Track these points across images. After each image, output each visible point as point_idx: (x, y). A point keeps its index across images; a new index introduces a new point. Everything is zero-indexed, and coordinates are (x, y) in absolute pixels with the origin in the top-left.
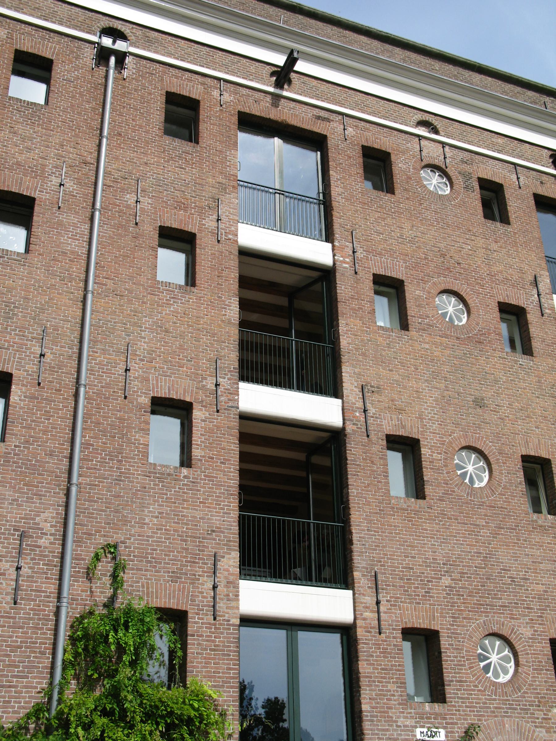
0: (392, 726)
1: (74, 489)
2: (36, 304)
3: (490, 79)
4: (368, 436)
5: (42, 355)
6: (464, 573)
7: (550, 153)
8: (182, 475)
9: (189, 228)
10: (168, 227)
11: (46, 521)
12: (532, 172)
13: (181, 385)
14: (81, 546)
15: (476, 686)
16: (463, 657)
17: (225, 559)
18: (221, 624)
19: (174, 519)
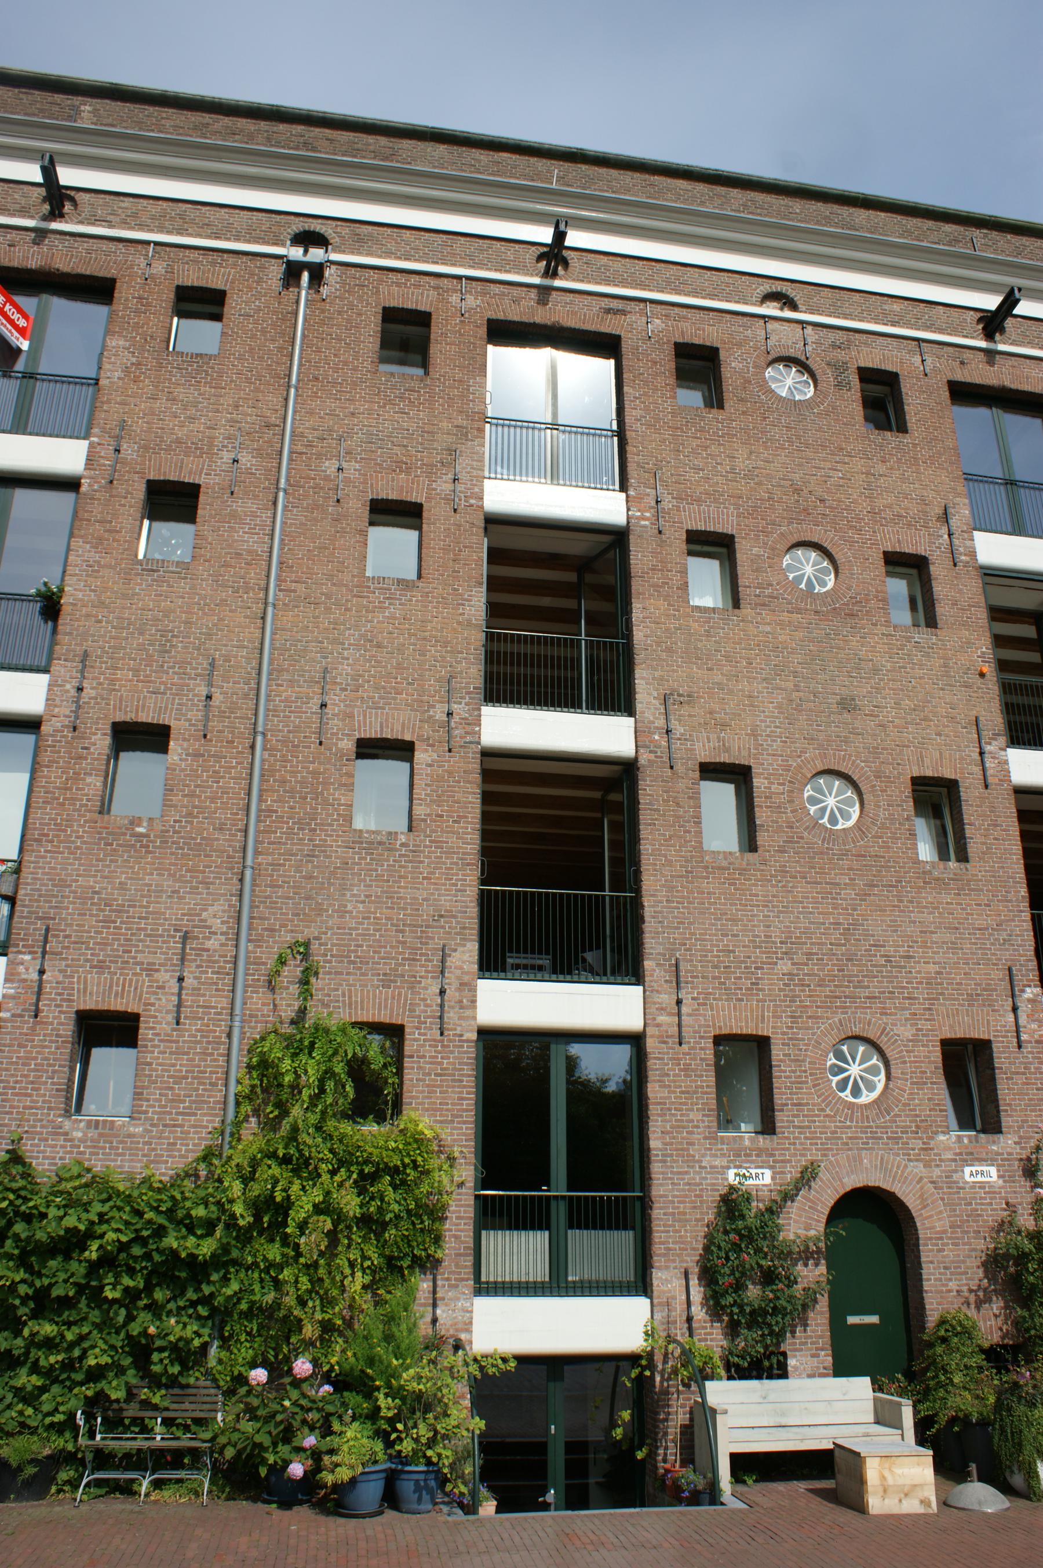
1: (248, 873)
3: (883, 214)
4: (672, 767)
5: (209, 697)
7: (979, 315)
9: (413, 497)
11: (215, 916)
12: (945, 348)
14: (261, 947)
15: (823, 1110)
18: (450, 1041)
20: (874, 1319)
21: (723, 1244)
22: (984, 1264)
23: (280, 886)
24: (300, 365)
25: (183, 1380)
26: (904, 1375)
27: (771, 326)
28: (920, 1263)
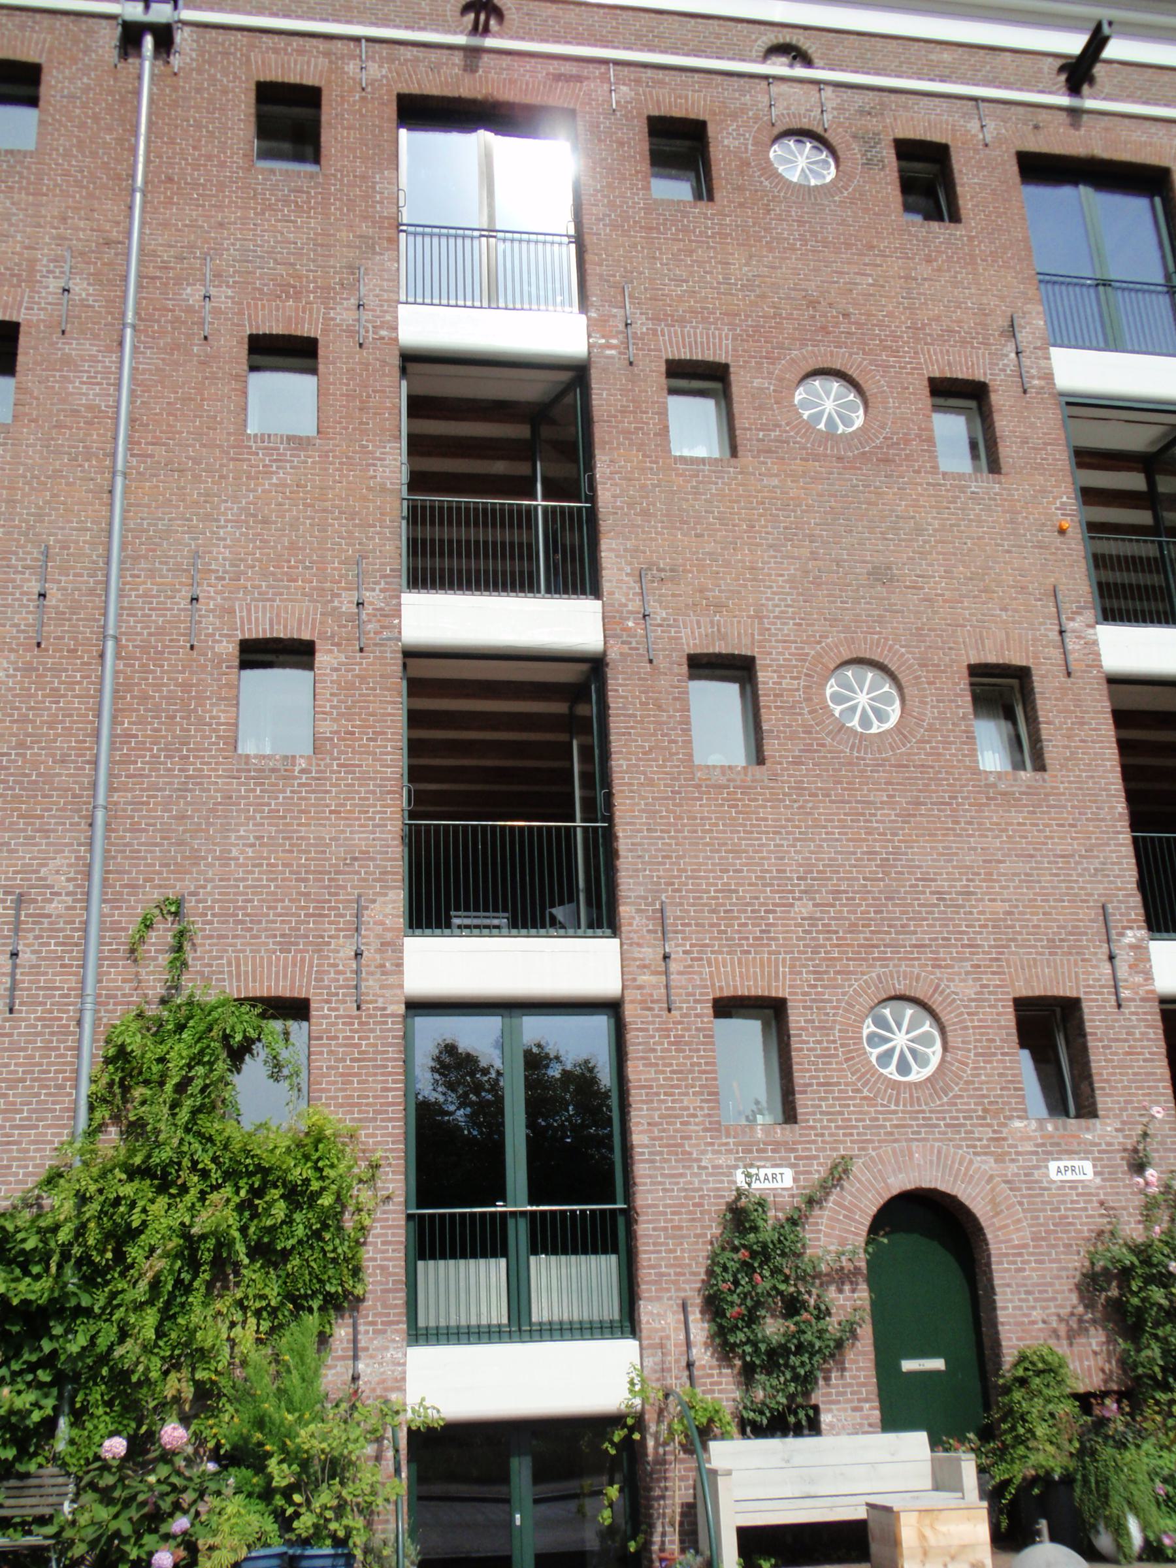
0: (690, 1167)
1: (100, 815)
2: (28, 508)
4: (651, 661)
6: (838, 892)
7: (1060, 62)
8: (297, 768)
10: (265, 335)
11: (57, 872)
12: (1013, 108)
13: (293, 613)
14: (120, 908)
16: (834, 1042)
17: (377, 905)
18: (370, 1016)
19: (283, 845)
20: (938, 1364)
21: (730, 1264)
22: (1078, 1286)
23: (144, 830)
24: (148, 161)
25: (21, 1468)
26: (977, 1434)
27: (775, 89)
28: (993, 1288)
